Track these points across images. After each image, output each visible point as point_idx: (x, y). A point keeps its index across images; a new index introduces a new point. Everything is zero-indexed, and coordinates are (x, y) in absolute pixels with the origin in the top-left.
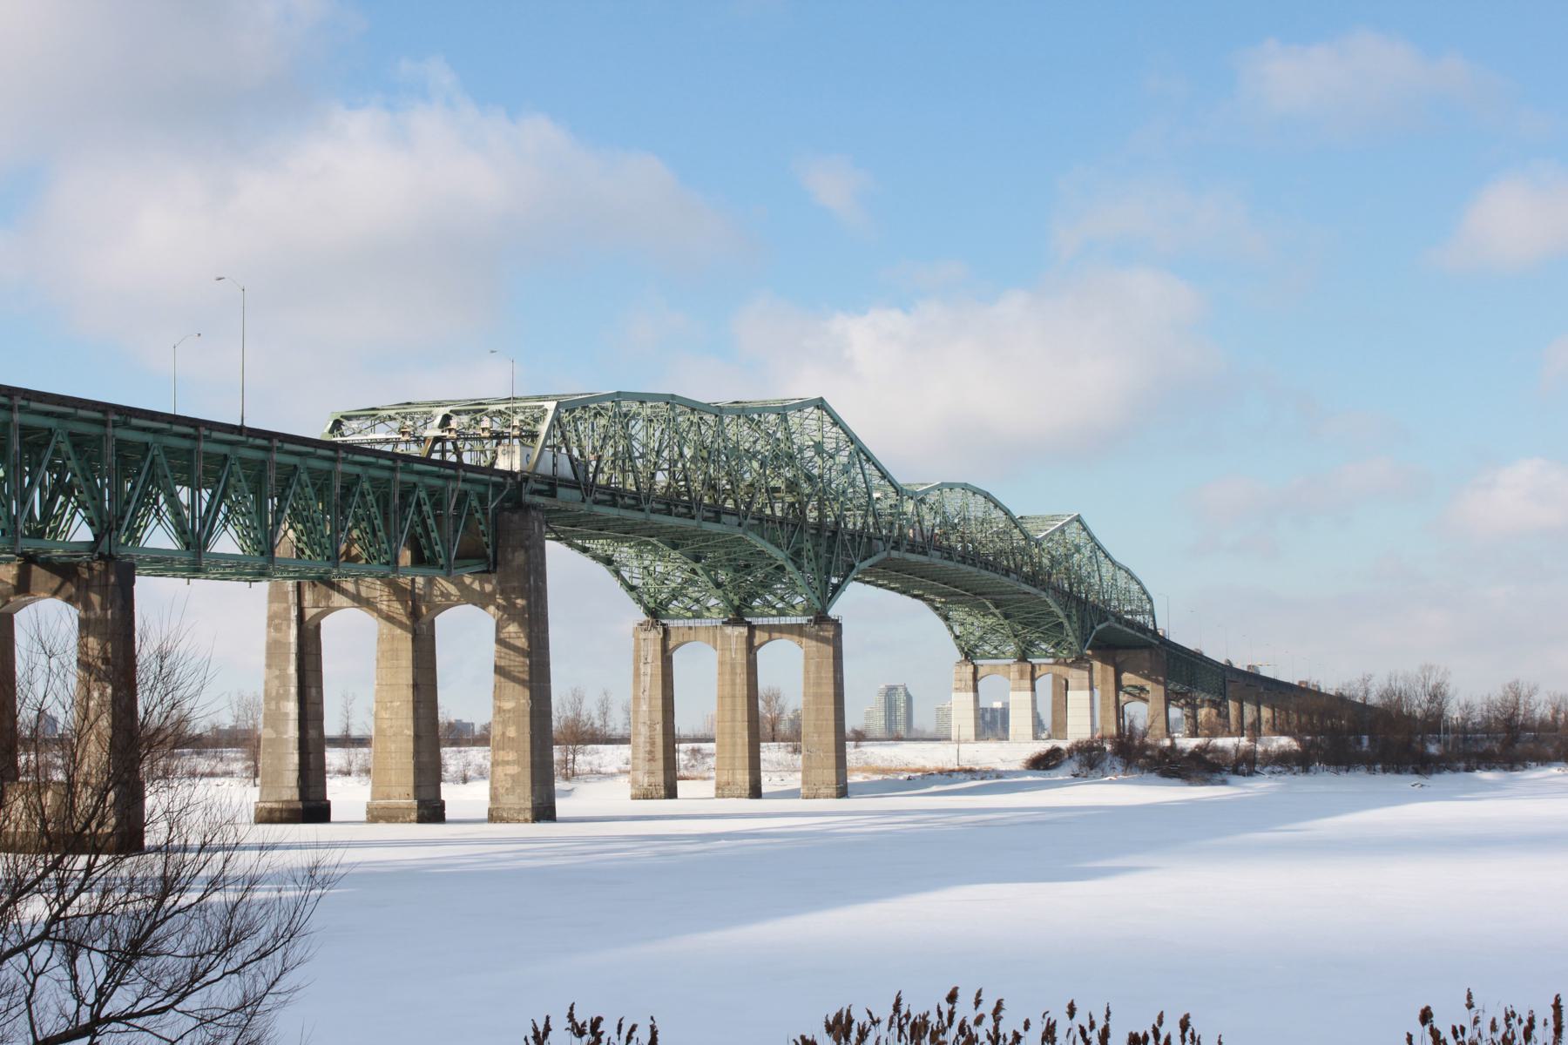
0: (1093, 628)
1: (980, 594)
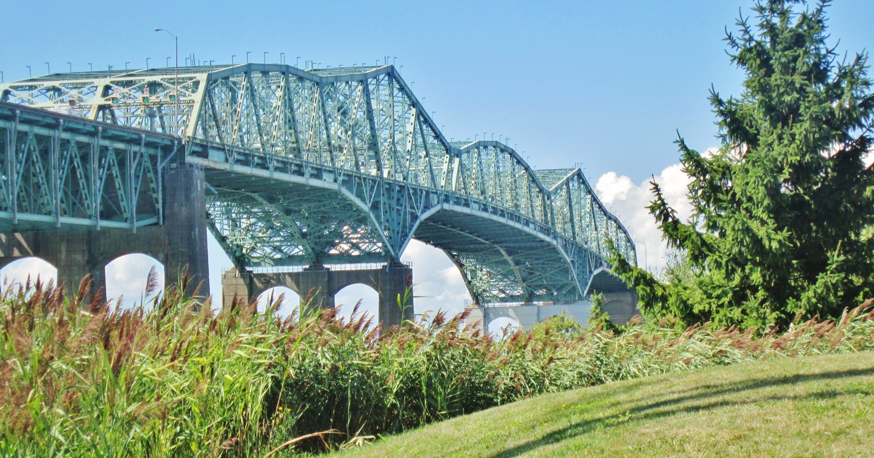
0: (591, 272)
1: (497, 243)
